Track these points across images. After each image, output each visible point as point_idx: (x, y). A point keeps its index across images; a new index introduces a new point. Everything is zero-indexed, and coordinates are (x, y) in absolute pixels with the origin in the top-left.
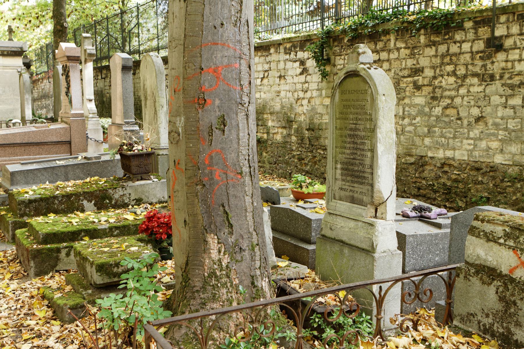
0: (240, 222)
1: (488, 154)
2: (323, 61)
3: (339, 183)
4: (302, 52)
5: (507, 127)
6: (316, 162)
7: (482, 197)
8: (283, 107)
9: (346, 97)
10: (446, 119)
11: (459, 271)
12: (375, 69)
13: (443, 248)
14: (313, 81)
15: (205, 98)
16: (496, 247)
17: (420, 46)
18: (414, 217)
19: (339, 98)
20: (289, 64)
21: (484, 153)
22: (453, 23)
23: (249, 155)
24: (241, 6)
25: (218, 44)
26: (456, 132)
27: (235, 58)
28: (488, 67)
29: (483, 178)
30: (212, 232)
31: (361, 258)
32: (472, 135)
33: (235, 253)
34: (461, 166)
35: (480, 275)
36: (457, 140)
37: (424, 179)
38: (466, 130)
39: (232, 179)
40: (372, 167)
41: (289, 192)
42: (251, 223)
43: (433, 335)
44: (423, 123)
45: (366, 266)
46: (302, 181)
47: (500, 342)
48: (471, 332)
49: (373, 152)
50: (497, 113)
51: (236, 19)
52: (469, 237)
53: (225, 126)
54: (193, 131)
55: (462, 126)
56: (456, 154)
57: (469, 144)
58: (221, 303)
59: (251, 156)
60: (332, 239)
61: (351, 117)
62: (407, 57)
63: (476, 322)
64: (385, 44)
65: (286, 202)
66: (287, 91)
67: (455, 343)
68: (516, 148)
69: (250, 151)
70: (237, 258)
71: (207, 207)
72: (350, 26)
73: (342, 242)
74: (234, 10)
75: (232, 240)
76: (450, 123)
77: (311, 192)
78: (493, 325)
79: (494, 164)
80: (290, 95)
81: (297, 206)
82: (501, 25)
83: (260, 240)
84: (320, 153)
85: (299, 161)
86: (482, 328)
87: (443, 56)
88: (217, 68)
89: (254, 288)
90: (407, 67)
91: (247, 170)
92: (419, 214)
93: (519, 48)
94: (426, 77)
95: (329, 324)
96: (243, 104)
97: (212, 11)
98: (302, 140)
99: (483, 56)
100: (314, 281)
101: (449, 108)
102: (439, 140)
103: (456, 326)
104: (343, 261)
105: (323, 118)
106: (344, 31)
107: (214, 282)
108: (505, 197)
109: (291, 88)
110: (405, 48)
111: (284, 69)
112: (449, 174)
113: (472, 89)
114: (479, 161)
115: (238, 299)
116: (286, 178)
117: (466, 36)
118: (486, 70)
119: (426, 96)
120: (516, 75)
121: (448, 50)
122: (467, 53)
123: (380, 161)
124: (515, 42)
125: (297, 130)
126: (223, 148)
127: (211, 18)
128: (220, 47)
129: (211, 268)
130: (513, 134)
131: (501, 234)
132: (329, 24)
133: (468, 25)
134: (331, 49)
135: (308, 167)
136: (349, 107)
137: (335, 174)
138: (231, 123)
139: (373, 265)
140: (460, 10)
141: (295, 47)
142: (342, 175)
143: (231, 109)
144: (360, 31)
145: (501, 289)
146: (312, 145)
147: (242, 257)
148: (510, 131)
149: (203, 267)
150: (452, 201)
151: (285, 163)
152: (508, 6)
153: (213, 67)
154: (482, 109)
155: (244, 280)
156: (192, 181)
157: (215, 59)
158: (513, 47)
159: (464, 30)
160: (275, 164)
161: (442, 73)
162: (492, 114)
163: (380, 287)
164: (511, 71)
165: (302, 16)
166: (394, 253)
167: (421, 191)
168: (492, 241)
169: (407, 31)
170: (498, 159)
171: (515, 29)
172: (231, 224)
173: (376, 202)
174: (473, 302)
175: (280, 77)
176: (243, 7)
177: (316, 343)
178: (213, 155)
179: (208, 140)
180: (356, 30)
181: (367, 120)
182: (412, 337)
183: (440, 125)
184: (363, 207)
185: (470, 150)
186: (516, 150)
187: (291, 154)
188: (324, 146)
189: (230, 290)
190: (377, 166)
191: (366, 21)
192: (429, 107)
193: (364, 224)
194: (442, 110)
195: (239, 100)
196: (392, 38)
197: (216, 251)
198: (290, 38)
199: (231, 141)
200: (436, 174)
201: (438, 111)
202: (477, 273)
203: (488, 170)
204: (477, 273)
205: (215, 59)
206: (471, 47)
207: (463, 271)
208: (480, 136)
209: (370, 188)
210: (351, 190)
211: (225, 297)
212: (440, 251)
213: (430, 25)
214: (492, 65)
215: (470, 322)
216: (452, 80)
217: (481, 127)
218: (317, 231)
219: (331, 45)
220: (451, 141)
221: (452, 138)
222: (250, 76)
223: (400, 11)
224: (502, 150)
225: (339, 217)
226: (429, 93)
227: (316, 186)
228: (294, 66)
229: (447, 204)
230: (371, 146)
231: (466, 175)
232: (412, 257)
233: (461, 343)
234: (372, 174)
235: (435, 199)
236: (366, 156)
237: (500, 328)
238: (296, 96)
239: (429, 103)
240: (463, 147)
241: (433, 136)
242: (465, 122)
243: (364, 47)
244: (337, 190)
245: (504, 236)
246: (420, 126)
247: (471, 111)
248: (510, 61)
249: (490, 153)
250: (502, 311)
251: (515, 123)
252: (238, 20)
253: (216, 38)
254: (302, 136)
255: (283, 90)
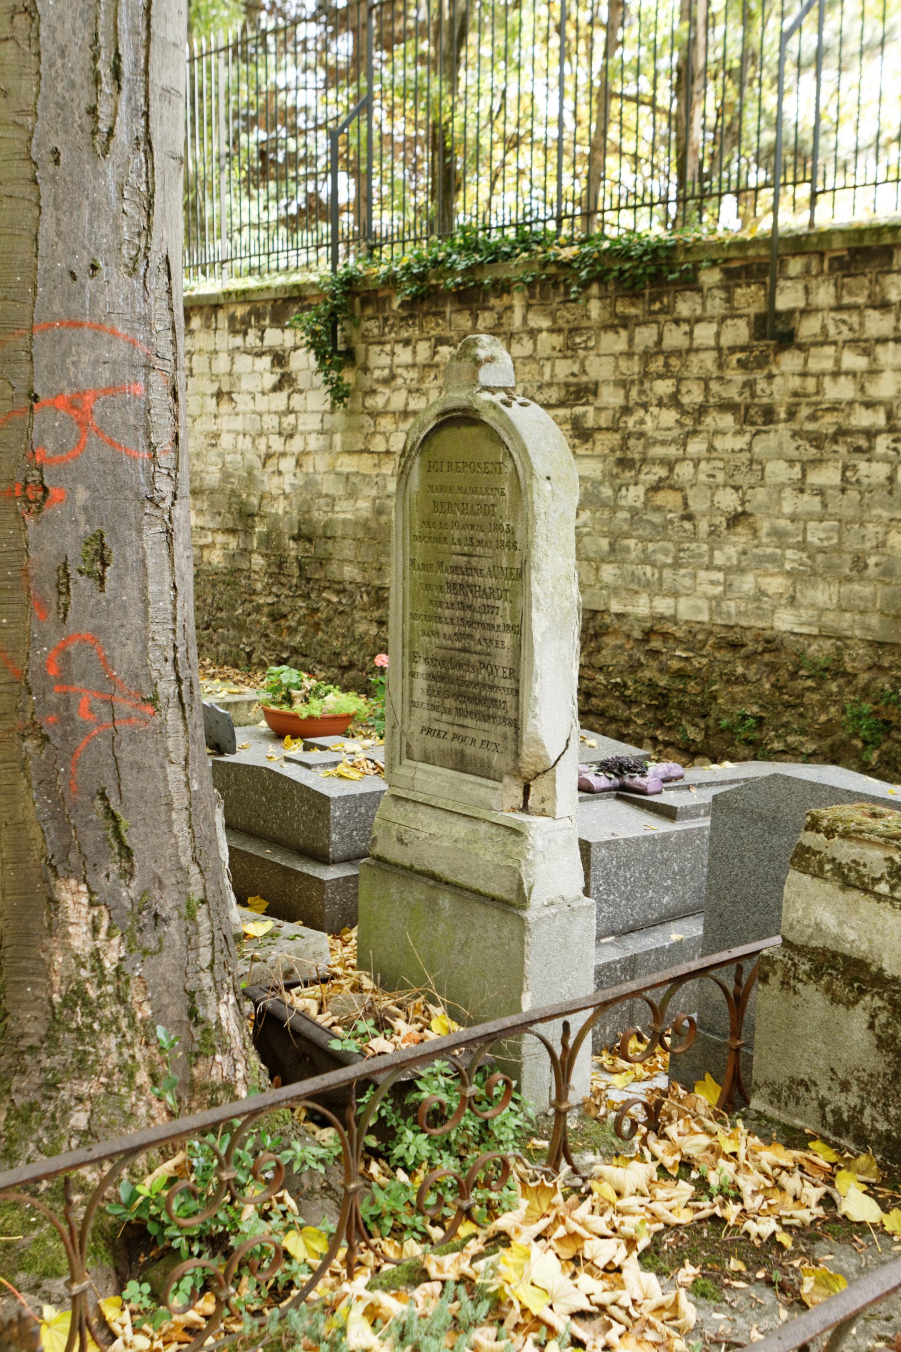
0: (154, 841)
1: (758, 608)
2: (336, 358)
3: (422, 715)
4: (279, 331)
5: (804, 541)
6: (318, 624)
7: (745, 717)
8: (226, 476)
9: (441, 479)
10: (656, 518)
11: (767, 968)
12: (522, 404)
13: (682, 870)
14: (309, 408)
15: (46, 483)
16: (866, 904)
17: (589, 328)
18: (604, 790)
19: (422, 482)
20: (244, 362)
21: (750, 606)
22: (671, 272)
23: (175, 648)
24: (149, 215)
25: (81, 325)
26: (680, 550)
27: (133, 366)
28: (758, 388)
29: (747, 668)
30: (71, 873)
31: (488, 922)
32: (719, 558)
33: (140, 930)
34: (693, 639)
35: (826, 978)
36: (682, 571)
37: (601, 669)
38: (705, 547)
39: (129, 718)
40: (514, 674)
41: (256, 712)
42: (184, 840)
43: (712, 1149)
44: (598, 527)
45: (503, 945)
46: (290, 685)
47: (879, 1157)
48: (801, 1130)
49: (519, 632)
50: (781, 506)
51: (134, 253)
52: (793, 876)
53: (105, 564)
54: (9, 579)
55: (694, 537)
56: (681, 608)
57: (713, 583)
58: (103, 1080)
59: (181, 649)
60: (403, 867)
61: (456, 536)
62: (556, 354)
63: (815, 1104)
64: (500, 318)
65: (253, 750)
66: (238, 433)
67: (769, 1169)
68: (827, 594)
69: (179, 634)
70: (146, 945)
71: (54, 802)
72: (408, 267)
73: (432, 876)
74: (129, 227)
75: (132, 895)
76: (665, 527)
77: (317, 713)
78: (861, 1112)
79: (774, 633)
80: (245, 443)
81: (288, 760)
82: (789, 283)
83: (211, 887)
84: (329, 602)
85: (274, 620)
86: (830, 1119)
87: (647, 356)
88: (81, 394)
89: (195, 1025)
90: (556, 380)
91: (171, 690)
92: (617, 781)
93: (835, 343)
94: (606, 408)
95: (411, 1112)
96: (157, 500)
97: (63, 228)
98: (280, 566)
99: (747, 358)
100: (357, 988)
101: (663, 488)
102: (639, 570)
103: (760, 1115)
104: (436, 930)
105: (337, 508)
106: (391, 280)
107: (79, 1019)
108: (801, 715)
109: (253, 428)
110: (551, 331)
111: (230, 374)
112: (663, 658)
113: (719, 443)
114: (737, 625)
115: (151, 1062)
116: (236, 666)
117: (704, 305)
118: (753, 395)
119: (604, 458)
120: (828, 410)
121: (659, 342)
122: (706, 349)
123: (537, 660)
124: (824, 327)
125: (266, 540)
126: (99, 630)
127: (60, 248)
128: (88, 334)
129: (69, 980)
130: (820, 558)
131: (881, 869)
132: (351, 262)
133: (710, 277)
134: (357, 325)
135: (298, 638)
136: (449, 506)
137: (411, 690)
138: (124, 556)
139: (523, 942)
140: (690, 240)
141: (259, 316)
142: (430, 692)
143: (124, 515)
144: (434, 282)
145: (882, 1018)
146: (309, 580)
147: (160, 941)
148: (813, 551)
149: (47, 977)
150: (670, 728)
151: (234, 626)
152: (808, 236)
153: (67, 393)
154: (744, 494)
155: (168, 1006)
156: (10, 725)
157: (73, 369)
158: (820, 339)
159: (699, 290)
160: (207, 628)
161: (644, 399)
162: (768, 507)
163: (566, 1025)
164: (814, 399)
165: (267, 229)
166: (575, 905)
167: (594, 701)
168: (857, 887)
169: (556, 285)
170: (785, 621)
171: (824, 295)
172: (128, 848)
173: (528, 769)
174: (805, 1051)
175: (219, 395)
176: (155, 219)
177: (374, 1168)
178: (72, 648)
179: (54, 606)
180: (422, 277)
181: (501, 544)
182: (654, 1158)
183: (640, 532)
184: (491, 783)
185: (715, 598)
186: (826, 598)
187: (251, 601)
188: (340, 583)
189: (129, 1038)
190: (531, 672)
191: (450, 255)
192: (611, 485)
193: (493, 830)
194: (646, 494)
195: (145, 489)
196: (518, 301)
197: (85, 928)
198: (244, 292)
199: (124, 607)
200: (630, 657)
201: (634, 495)
202: (817, 972)
203: (760, 649)
204: (817, 972)
205: (73, 369)
206: (718, 335)
207: (778, 966)
208: (739, 561)
209: (509, 731)
210: (455, 736)
211: (115, 1061)
212: (674, 880)
213: (615, 274)
214: (770, 384)
215: (797, 1103)
216: (669, 417)
217: (743, 540)
218: (344, 828)
219: (358, 313)
220: (667, 573)
221: (669, 566)
222: (176, 418)
223: (535, 234)
224: (793, 598)
225: (423, 808)
226: (612, 450)
227: (330, 698)
228: (256, 368)
229: (660, 735)
230: (513, 617)
231: (705, 661)
232: (606, 901)
233: (783, 1168)
234: (517, 692)
235: (628, 722)
236: (498, 644)
237: (881, 1119)
238: (263, 449)
239: (611, 475)
240: (699, 588)
241: (623, 561)
242: (703, 526)
243: (490, 345)
244: (417, 734)
245: (890, 874)
246: (589, 534)
247: (716, 499)
248: (812, 375)
249: (765, 606)
250: (885, 1074)
251: (825, 530)
252: (141, 256)
253: (75, 306)
254: (281, 556)
255: (228, 431)
